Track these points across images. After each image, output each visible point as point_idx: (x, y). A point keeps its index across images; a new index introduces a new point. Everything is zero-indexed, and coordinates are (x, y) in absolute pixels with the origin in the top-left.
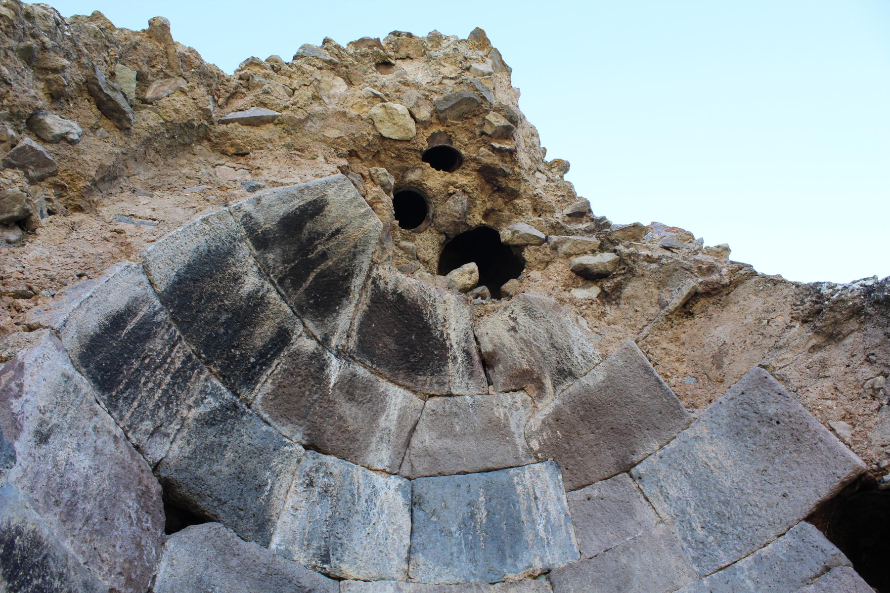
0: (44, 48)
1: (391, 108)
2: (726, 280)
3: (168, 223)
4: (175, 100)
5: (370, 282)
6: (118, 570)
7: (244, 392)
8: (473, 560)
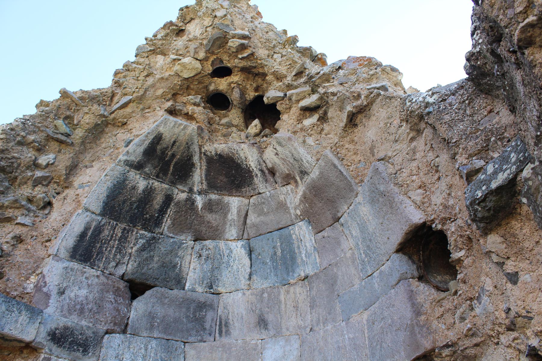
0: (24, 137)
1: (182, 63)
2: (365, 103)
3: (93, 183)
4: (86, 118)
5: (203, 155)
6: (109, 322)
7: (157, 230)
8: (276, 275)
